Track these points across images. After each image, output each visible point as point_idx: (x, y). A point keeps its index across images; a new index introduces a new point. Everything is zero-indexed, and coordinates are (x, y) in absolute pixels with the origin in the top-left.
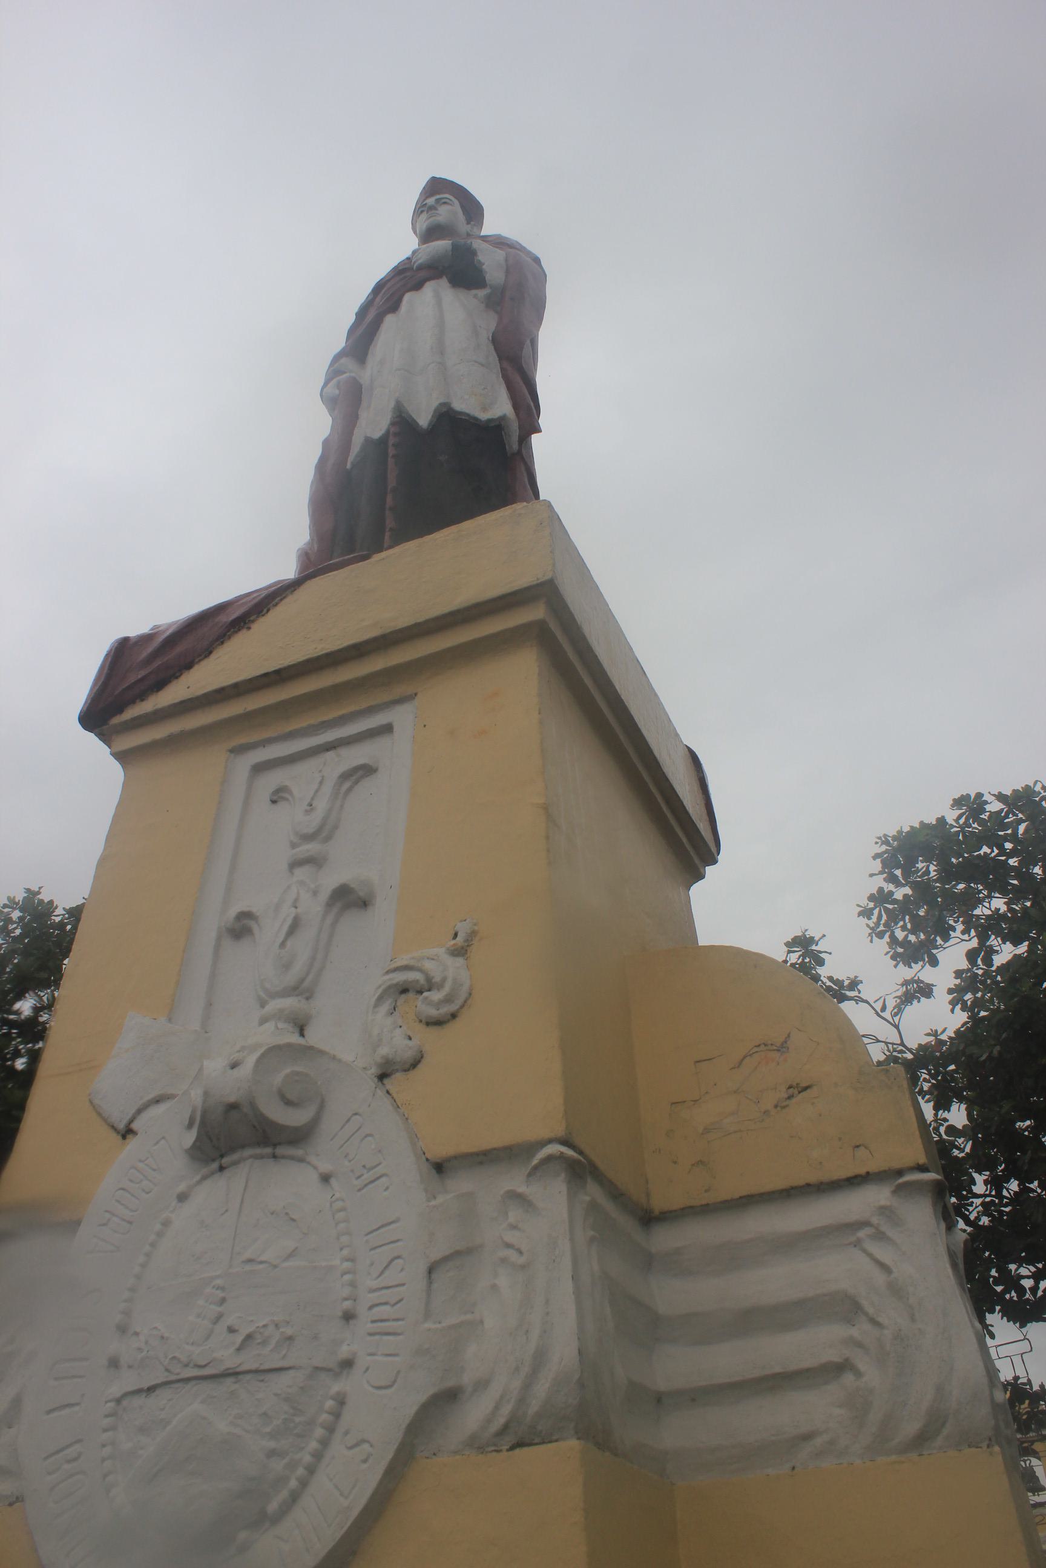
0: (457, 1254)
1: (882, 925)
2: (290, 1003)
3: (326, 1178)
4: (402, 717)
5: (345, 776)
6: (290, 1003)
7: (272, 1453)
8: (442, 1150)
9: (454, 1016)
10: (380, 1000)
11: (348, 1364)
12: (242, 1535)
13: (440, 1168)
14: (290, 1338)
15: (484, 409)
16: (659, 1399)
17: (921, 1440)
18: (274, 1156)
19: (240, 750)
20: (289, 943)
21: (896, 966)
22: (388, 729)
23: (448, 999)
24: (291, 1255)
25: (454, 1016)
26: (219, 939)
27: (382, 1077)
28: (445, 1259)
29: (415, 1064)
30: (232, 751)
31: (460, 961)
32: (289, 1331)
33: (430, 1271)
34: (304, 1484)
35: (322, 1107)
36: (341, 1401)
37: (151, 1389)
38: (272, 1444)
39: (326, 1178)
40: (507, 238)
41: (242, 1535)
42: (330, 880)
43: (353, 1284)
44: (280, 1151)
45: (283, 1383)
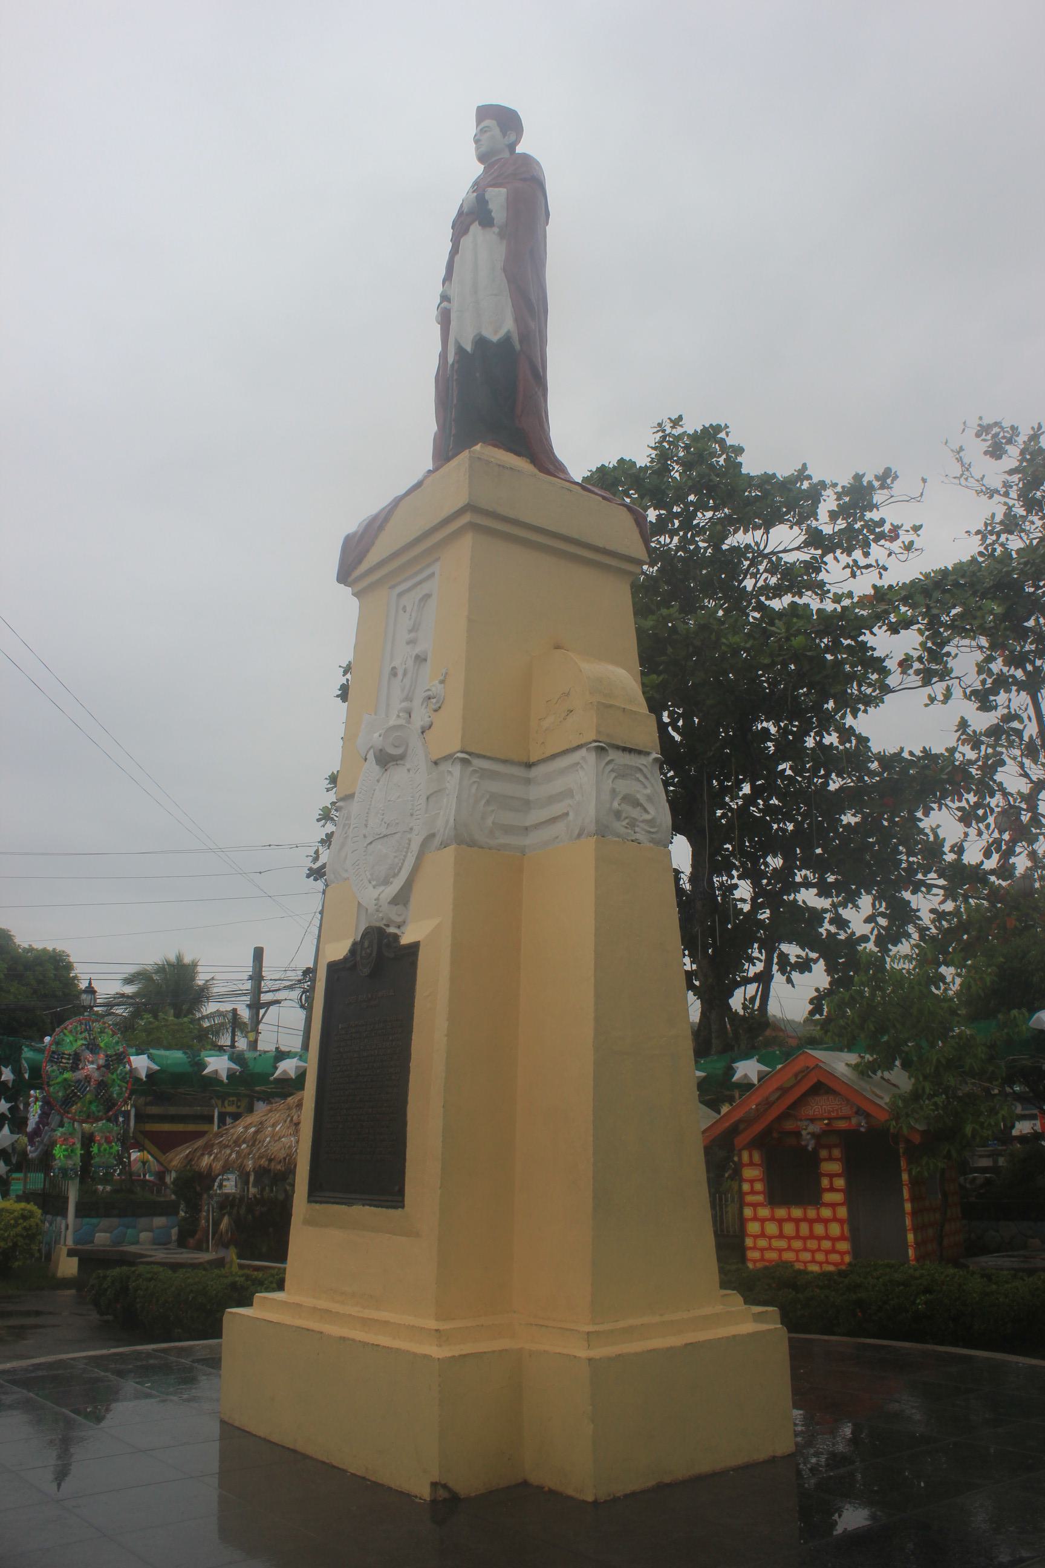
0: (436, 792)
1: (990, 435)
2: (404, 704)
3: (409, 770)
4: (436, 568)
5: (421, 600)
6: (404, 704)
7: (395, 857)
8: (435, 758)
9: (440, 707)
10: (422, 704)
11: (411, 829)
12: (391, 879)
13: (436, 763)
14: (398, 823)
15: (496, 332)
16: (526, 828)
17: (579, 836)
18: (397, 764)
19: (392, 587)
20: (404, 680)
21: (326, 779)
22: (433, 575)
23: (437, 702)
24: (399, 797)
25: (440, 707)
26: (389, 679)
27: (423, 733)
28: (431, 794)
29: (430, 727)
30: (390, 588)
31: (443, 685)
32: (397, 821)
33: (428, 798)
34: (402, 864)
35: (407, 746)
36: (410, 840)
37: (371, 843)
38: (395, 854)
39: (409, 770)
40: (530, 156)
41: (391, 879)
42: (418, 650)
43: (413, 805)
44: (398, 762)
45: (397, 836)
